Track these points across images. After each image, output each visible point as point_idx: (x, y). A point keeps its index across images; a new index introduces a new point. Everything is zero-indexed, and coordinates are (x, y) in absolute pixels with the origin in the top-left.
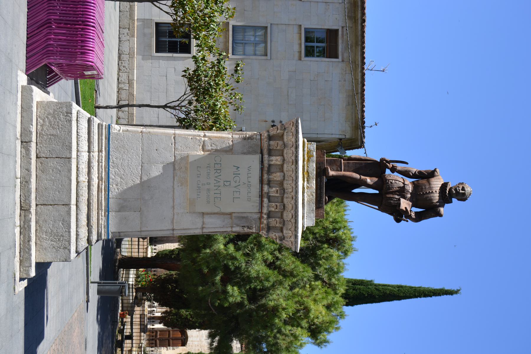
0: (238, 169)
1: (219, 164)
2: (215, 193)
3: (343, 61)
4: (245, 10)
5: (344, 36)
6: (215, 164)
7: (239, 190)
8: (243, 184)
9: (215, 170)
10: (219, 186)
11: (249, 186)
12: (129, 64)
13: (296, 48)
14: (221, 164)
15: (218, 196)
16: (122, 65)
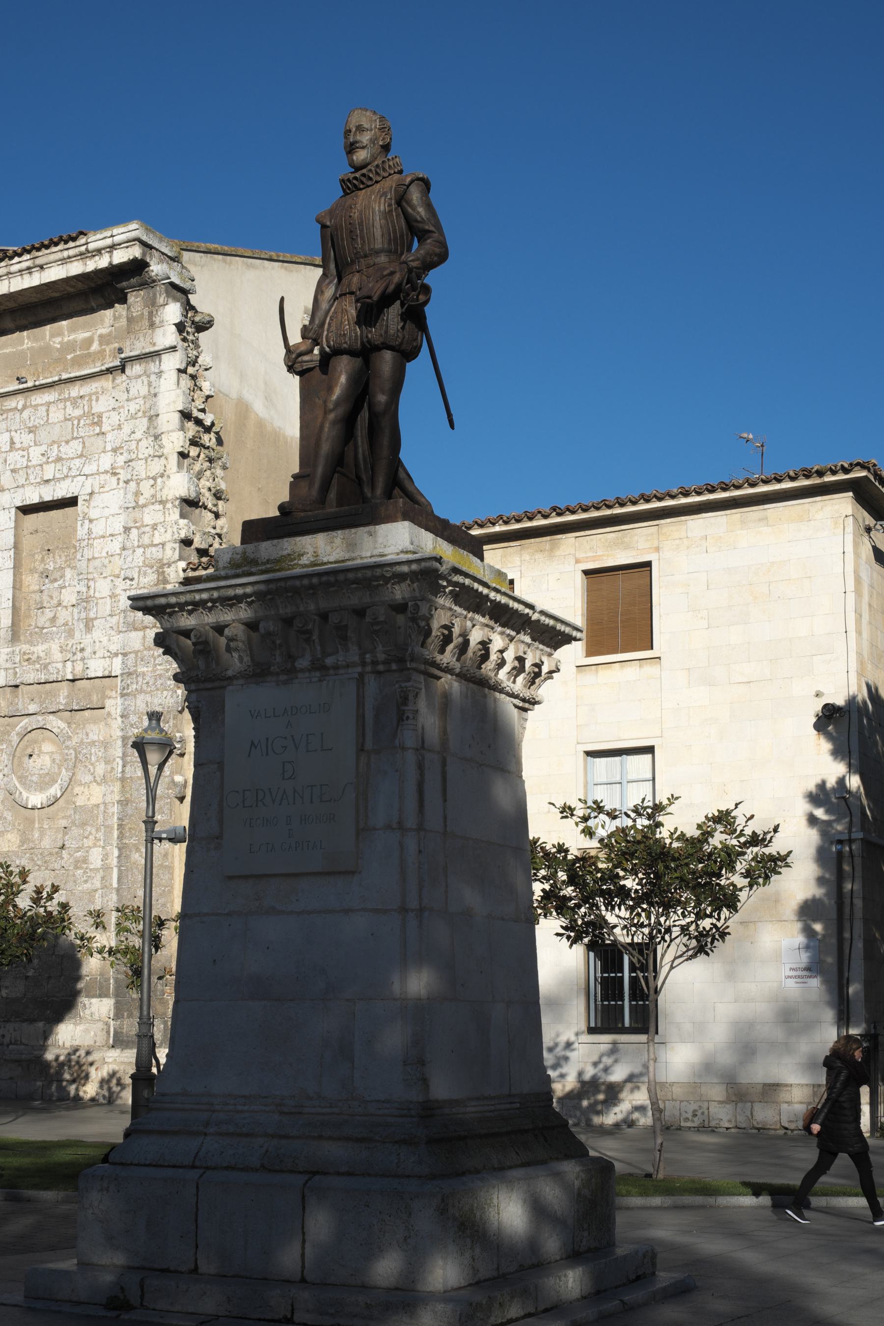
0: (256, 743)
1: (244, 796)
2: (312, 802)
3: (657, 549)
4: (549, 812)
5: (598, 554)
6: (244, 807)
8: (289, 727)
9: (257, 806)
10: (295, 791)
11: (294, 713)
12: (688, 1101)
13: (631, 672)
14: (244, 791)
16: (690, 1118)
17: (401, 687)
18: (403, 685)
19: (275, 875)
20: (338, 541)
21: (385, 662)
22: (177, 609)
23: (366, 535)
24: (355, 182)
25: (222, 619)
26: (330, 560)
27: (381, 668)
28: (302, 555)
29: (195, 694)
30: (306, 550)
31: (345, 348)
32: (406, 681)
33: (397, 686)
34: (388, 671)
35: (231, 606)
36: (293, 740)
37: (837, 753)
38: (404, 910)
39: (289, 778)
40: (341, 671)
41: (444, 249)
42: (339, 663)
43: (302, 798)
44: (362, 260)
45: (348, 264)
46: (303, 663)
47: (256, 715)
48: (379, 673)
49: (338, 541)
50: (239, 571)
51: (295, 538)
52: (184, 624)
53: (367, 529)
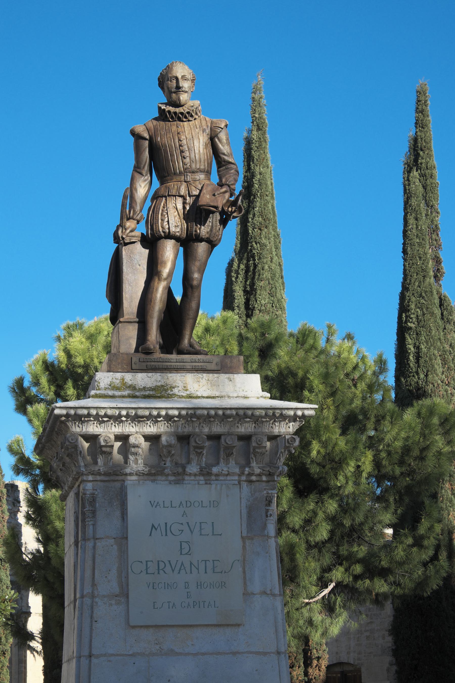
2: (206, 572)
6: (147, 573)
7: (198, 524)
10: (191, 564)
14: (147, 561)
15: (210, 565)
17: (268, 493)
18: (270, 492)
19: (197, 626)
20: (203, 382)
21: (260, 475)
22: (92, 419)
23: (227, 380)
24: (180, 115)
25: (127, 430)
26: (203, 395)
27: (254, 478)
28: (174, 388)
29: (91, 484)
30: (177, 385)
31: (177, 235)
32: (272, 489)
33: (265, 492)
34: (258, 481)
35: (139, 422)
36: (189, 526)
37: (6, 553)
38: (279, 653)
39: (186, 554)
40: (221, 478)
41: (220, 173)
42: (223, 472)
43: (198, 569)
44: (189, 174)
45: (175, 174)
46: (193, 468)
47: (155, 504)
48: (251, 482)
49: (203, 382)
50: (117, 393)
51: (167, 374)
52: (92, 430)
53: (227, 375)
